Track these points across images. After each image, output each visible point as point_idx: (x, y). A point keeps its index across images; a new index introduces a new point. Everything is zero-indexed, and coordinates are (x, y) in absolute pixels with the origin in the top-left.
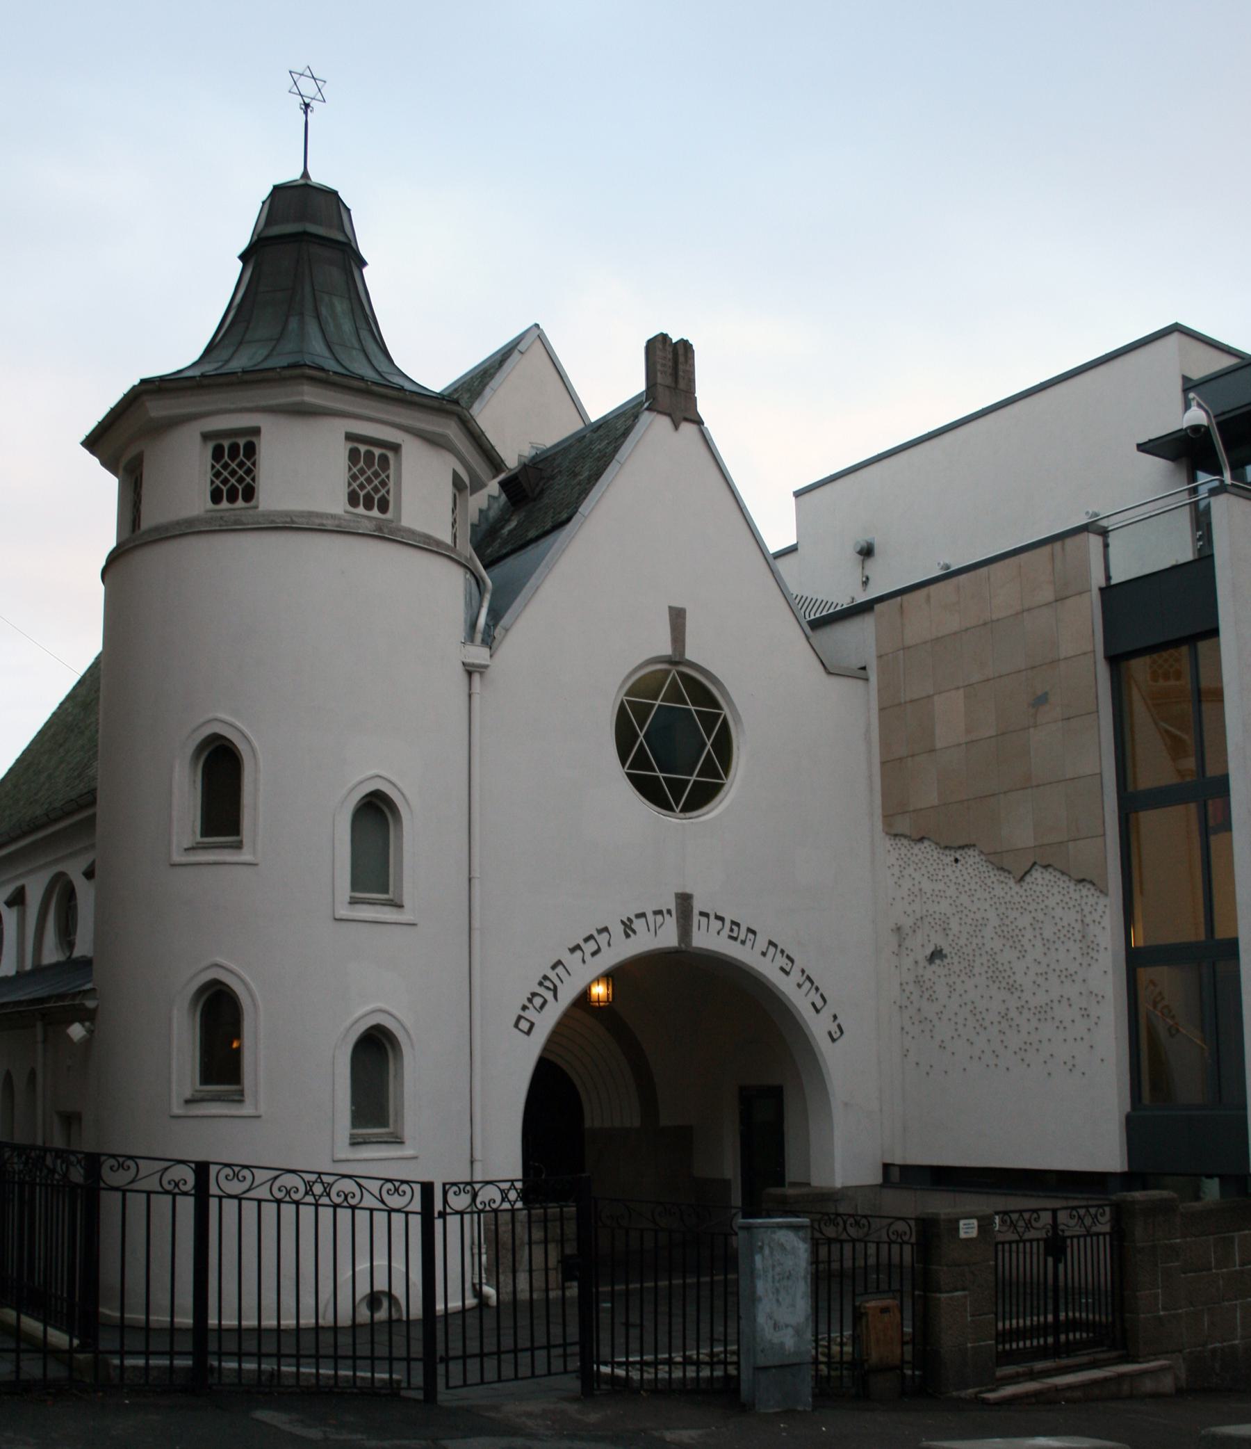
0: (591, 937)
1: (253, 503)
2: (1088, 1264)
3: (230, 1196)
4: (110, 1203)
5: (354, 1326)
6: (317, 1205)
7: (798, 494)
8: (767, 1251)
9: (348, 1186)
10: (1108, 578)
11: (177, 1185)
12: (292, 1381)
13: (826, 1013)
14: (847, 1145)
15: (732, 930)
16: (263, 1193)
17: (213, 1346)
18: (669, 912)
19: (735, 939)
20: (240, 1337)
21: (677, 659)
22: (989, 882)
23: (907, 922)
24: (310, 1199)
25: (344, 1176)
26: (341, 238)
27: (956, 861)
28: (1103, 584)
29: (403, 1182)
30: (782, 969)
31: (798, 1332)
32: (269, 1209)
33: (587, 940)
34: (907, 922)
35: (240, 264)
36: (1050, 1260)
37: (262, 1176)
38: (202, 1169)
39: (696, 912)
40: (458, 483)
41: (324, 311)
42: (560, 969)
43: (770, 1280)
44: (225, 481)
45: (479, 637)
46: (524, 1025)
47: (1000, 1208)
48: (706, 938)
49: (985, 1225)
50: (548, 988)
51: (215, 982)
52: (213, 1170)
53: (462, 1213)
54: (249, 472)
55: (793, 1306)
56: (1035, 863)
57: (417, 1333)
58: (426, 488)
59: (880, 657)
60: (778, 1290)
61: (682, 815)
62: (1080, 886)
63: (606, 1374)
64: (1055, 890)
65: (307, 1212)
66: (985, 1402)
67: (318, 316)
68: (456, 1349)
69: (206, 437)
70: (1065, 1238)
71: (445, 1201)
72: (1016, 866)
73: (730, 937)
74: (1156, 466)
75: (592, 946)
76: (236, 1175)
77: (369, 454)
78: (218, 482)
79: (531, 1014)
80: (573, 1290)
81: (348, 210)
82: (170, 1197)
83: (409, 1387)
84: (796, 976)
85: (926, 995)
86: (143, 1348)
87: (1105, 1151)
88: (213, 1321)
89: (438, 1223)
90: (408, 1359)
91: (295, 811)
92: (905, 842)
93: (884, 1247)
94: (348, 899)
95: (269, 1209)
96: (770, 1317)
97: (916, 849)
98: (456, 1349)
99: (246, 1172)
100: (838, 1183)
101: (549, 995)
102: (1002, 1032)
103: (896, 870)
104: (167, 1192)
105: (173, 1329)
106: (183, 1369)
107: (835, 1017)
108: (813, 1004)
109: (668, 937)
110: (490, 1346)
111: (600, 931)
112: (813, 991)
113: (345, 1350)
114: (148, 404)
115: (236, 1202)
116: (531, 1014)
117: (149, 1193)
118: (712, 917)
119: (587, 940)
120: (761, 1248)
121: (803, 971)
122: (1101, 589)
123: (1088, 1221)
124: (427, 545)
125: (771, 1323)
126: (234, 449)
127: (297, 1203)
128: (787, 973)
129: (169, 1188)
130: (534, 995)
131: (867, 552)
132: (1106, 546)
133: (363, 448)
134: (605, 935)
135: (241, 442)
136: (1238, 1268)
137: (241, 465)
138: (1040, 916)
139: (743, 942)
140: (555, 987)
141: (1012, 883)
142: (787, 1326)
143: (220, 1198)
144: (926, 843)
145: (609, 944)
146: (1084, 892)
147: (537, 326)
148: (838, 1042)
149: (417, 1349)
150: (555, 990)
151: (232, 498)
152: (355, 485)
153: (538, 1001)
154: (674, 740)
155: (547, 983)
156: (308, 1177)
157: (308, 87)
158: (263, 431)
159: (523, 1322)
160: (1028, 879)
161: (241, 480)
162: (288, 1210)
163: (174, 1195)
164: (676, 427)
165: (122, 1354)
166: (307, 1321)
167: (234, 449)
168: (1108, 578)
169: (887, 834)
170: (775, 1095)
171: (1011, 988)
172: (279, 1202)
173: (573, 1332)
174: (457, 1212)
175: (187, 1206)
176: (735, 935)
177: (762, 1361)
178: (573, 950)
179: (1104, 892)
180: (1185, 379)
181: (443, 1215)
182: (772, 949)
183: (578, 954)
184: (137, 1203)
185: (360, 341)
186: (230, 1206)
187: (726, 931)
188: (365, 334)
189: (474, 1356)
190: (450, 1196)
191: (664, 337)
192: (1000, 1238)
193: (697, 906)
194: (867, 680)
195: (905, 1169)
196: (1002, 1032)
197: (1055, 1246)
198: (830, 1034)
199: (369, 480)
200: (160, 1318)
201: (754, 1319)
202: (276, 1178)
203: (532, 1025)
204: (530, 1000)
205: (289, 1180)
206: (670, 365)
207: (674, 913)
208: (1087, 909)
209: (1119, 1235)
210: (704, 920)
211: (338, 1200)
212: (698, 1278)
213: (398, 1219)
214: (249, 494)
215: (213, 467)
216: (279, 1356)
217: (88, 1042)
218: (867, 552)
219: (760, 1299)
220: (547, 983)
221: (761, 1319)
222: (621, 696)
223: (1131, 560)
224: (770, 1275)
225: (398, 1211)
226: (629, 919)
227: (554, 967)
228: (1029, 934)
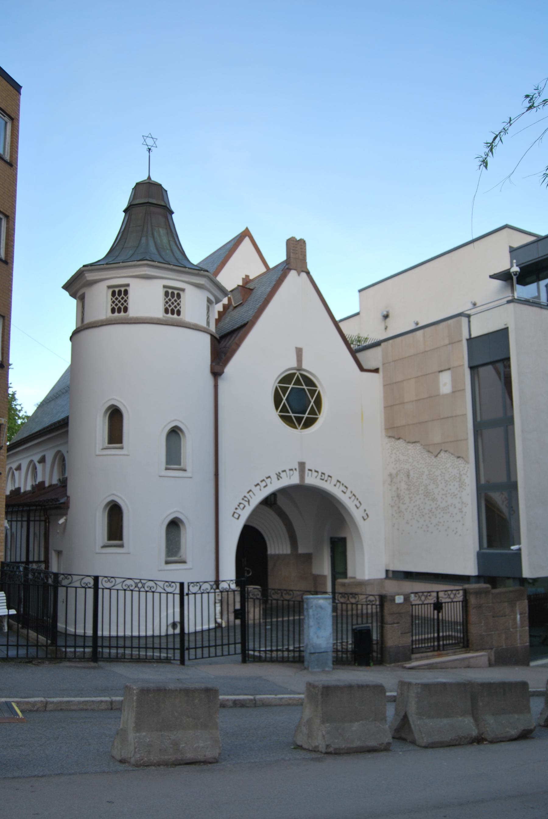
0: (264, 480)
1: (127, 314)
2: (453, 612)
3: (107, 588)
4: (61, 591)
5: (167, 635)
6: (139, 591)
7: (360, 291)
9: (151, 584)
10: (470, 335)
11: (87, 584)
13: (362, 509)
14: (369, 563)
16: (119, 587)
17: (99, 643)
18: (296, 469)
19: (323, 480)
20: (84, 640)
21: (299, 368)
22: (424, 456)
23: (394, 472)
24: (137, 589)
26: (163, 204)
28: (468, 337)
29: (172, 582)
30: (343, 491)
32: (121, 593)
33: (262, 481)
34: (394, 472)
35: (124, 214)
36: (436, 612)
37: (118, 580)
38: (96, 579)
40: (209, 301)
41: (156, 234)
42: (251, 493)
44: (116, 305)
46: (236, 516)
47: (416, 590)
48: (311, 480)
49: (407, 598)
50: (246, 501)
51: (113, 501)
52: (100, 579)
53: (195, 594)
54: (125, 301)
56: (441, 450)
57: (178, 640)
58: (195, 305)
59: (383, 364)
62: (459, 459)
63: (251, 655)
65: (136, 594)
66: (405, 668)
67: (153, 234)
68: (192, 645)
69: (109, 287)
70: (442, 603)
71: (189, 589)
72: (434, 450)
73: (321, 479)
74: (497, 283)
75: (264, 484)
76: (109, 581)
77: (173, 293)
78: (114, 305)
79: (239, 511)
80: (238, 622)
81: (166, 191)
82: (84, 589)
83: (174, 660)
84: (348, 494)
85: (401, 502)
86: (64, 645)
87: (470, 568)
88: (100, 633)
89: (186, 598)
90: (174, 649)
91: (144, 435)
92: (393, 439)
93: (364, 607)
94: (164, 468)
95: (121, 593)
97: (398, 442)
98: (192, 645)
99: (112, 579)
100: (367, 577)
101: (246, 504)
102: (430, 518)
104: (83, 587)
105: (84, 637)
106: (89, 652)
107: (365, 510)
109: (295, 480)
110: (219, 642)
111: (267, 478)
112: (356, 500)
113: (157, 646)
114: (86, 275)
115: (108, 590)
116: (239, 511)
117: (76, 588)
119: (262, 481)
121: (351, 492)
122: (467, 340)
123: (423, 598)
126: (120, 292)
127: (132, 591)
128: (345, 493)
129: (83, 585)
130: (240, 503)
131: (386, 317)
132: (469, 322)
133: (170, 291)
134: (269, 479)
135: (123, 289)
137: (122, 298)
138: (443, 471)
139: (326, 481)
141: (433, 457)
143: (103, 589)
144: (401, 440)
145: (271, 483)
146: (460, 462)
148: (366, 521)
149: (178, 646)
150: (249, 502)
151: (119, 312)
153: (242, 506)
154: (298, 400)
157: (150, 142)
158: (131, 285)
159: (232, 634)
160: (439, 456)
161: (122, 304)
162: (128, 593)
164: (299, 275)
165: (66, 647)
166: (150, 633)
167: (120, 292)
168: (470, 335)
169: (387, 436)
170: (343, 540)
171: (434, 500)
172: (125, 590)
173: (239, 640)
174: (193, 593)
175: (90, 593)
176: (323, 478)
178: (256, 486)
179: (467, 462)
180: (510, 247)
181: (188, 594)
182: (338, 484)
183: (258, 487)
184: (71, 591)
185: (170, 246)
186: (107, 592)
187: (319, 477)
188: (172, 243)
189: (206, 647)
190: (191, 588)
192: (414, 603)
193: (307, 467)
195: (394, 572)
196: (430, 518)
197: (438, 606)
198: (363, 517)
199: (173, 303)
200: (80, 631)
202: (124, 581)
203: (239, 515)
204: (239, 506)
205: (129, 582)
206: (296, 250)
208: (461, 469)
209: (465, 602)
210: (310, 472)
211: (147, 589)
213: (171, 596)
214: (126, 310)
215: (112, 299)
216: (125, 647)
218: (386, 317)
220: (246, 499)
222: (277, 384)
223: (481, 327)
225: (171, 593)
226: (279, 473)
227: (248, 492)
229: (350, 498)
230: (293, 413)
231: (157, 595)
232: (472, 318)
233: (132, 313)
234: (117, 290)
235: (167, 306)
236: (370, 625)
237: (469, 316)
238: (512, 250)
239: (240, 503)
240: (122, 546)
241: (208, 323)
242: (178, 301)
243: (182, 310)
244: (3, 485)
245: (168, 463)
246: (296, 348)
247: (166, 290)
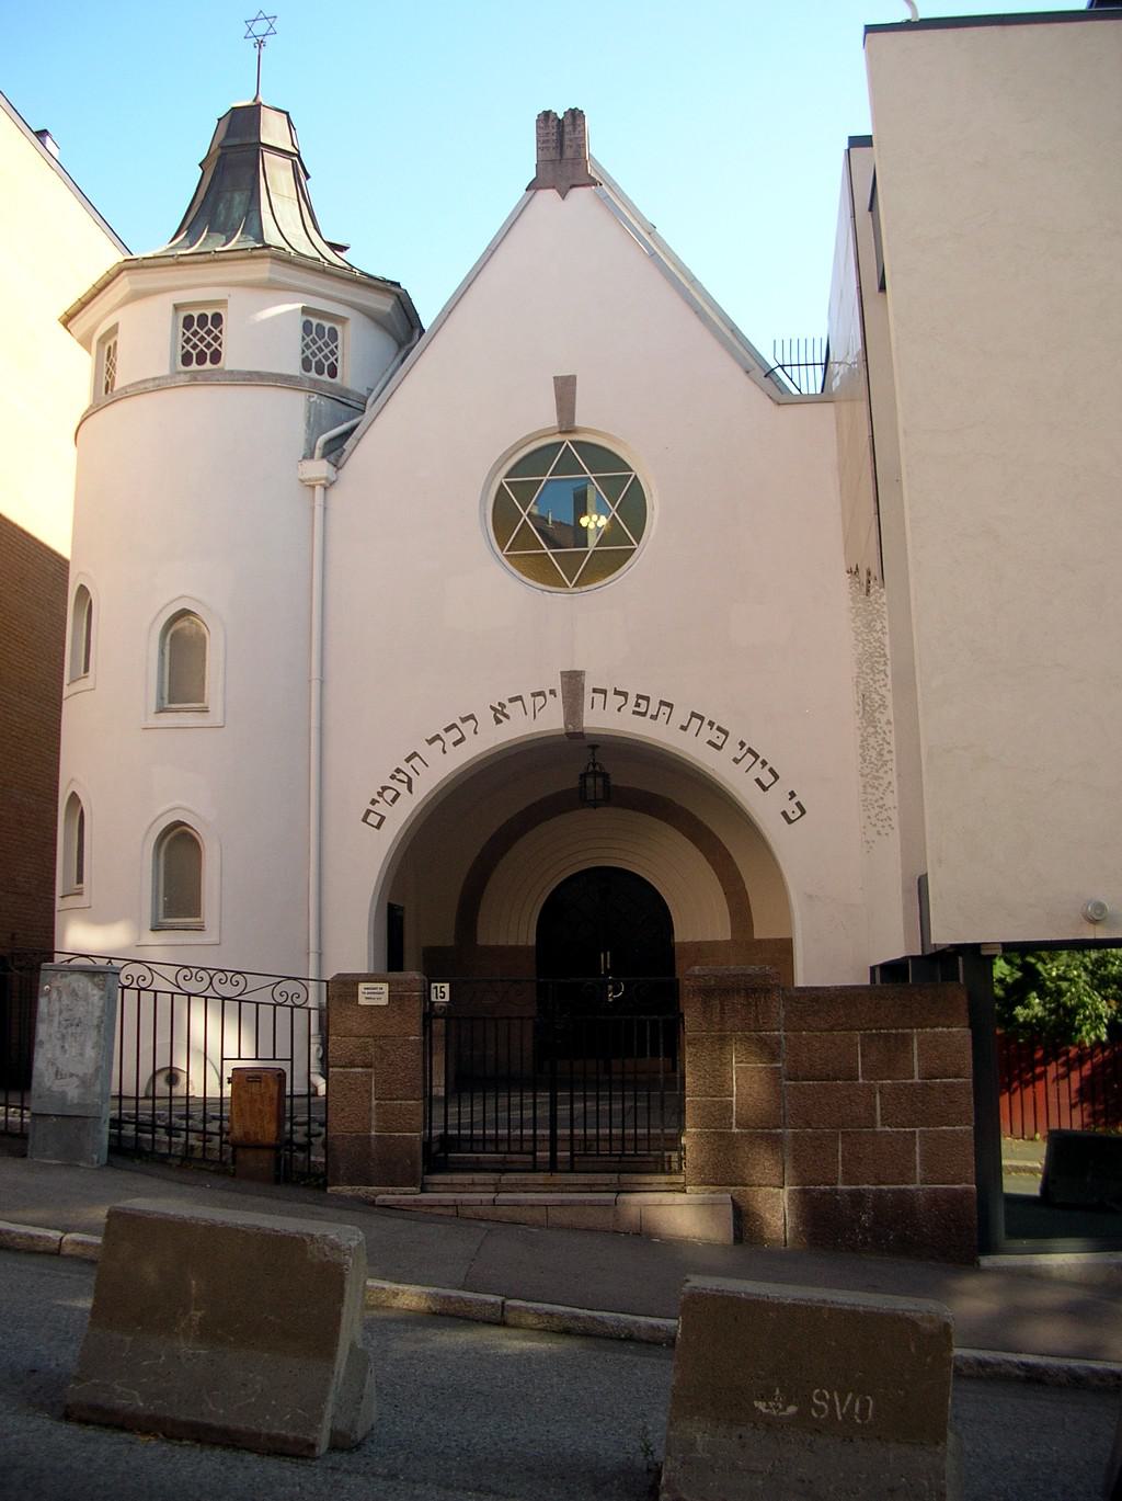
0: (454, 726)
8: (54, 995)
15: (638, 705)
19: (644, 714)
25: (289, 978)
33: (447, 730)
43: (56, 1024)
44: (195, 347)
45: (318, 453)
48: (600, 719)
60: (63, 1037)
61: (576, 589)
75: (455, 735)
79: (381, 808)
84: (732, 749)
101: (402, 788)
108: (758, 781)
109: (552, 720)
111: (464, 720)
116: (381, 808)
119: (447, 730)
125: (52, 1071)
130: (384, 788)
133: (315, 321)
135: (209, 313)
136: (917, 1080)
140: (410, 779)
142: (72, 1075)
152: (308, 353)
153: (389, 795)
163: (275, 1006)
178: (430, 742)
183: (439, 742)
193: (589, 683)
207: (559, 693)
210: (599, 697)
212: (572, 1092)
219: (42, 1043)
224: (56, 1020)
227: (408, 760)
229: (736, 761)
230: (548, 481)
234: (196, 314)
236: (286, 1066)
242: (333, 346)
243: (339, 366)
246: (563, 198)
247: (305, 318)
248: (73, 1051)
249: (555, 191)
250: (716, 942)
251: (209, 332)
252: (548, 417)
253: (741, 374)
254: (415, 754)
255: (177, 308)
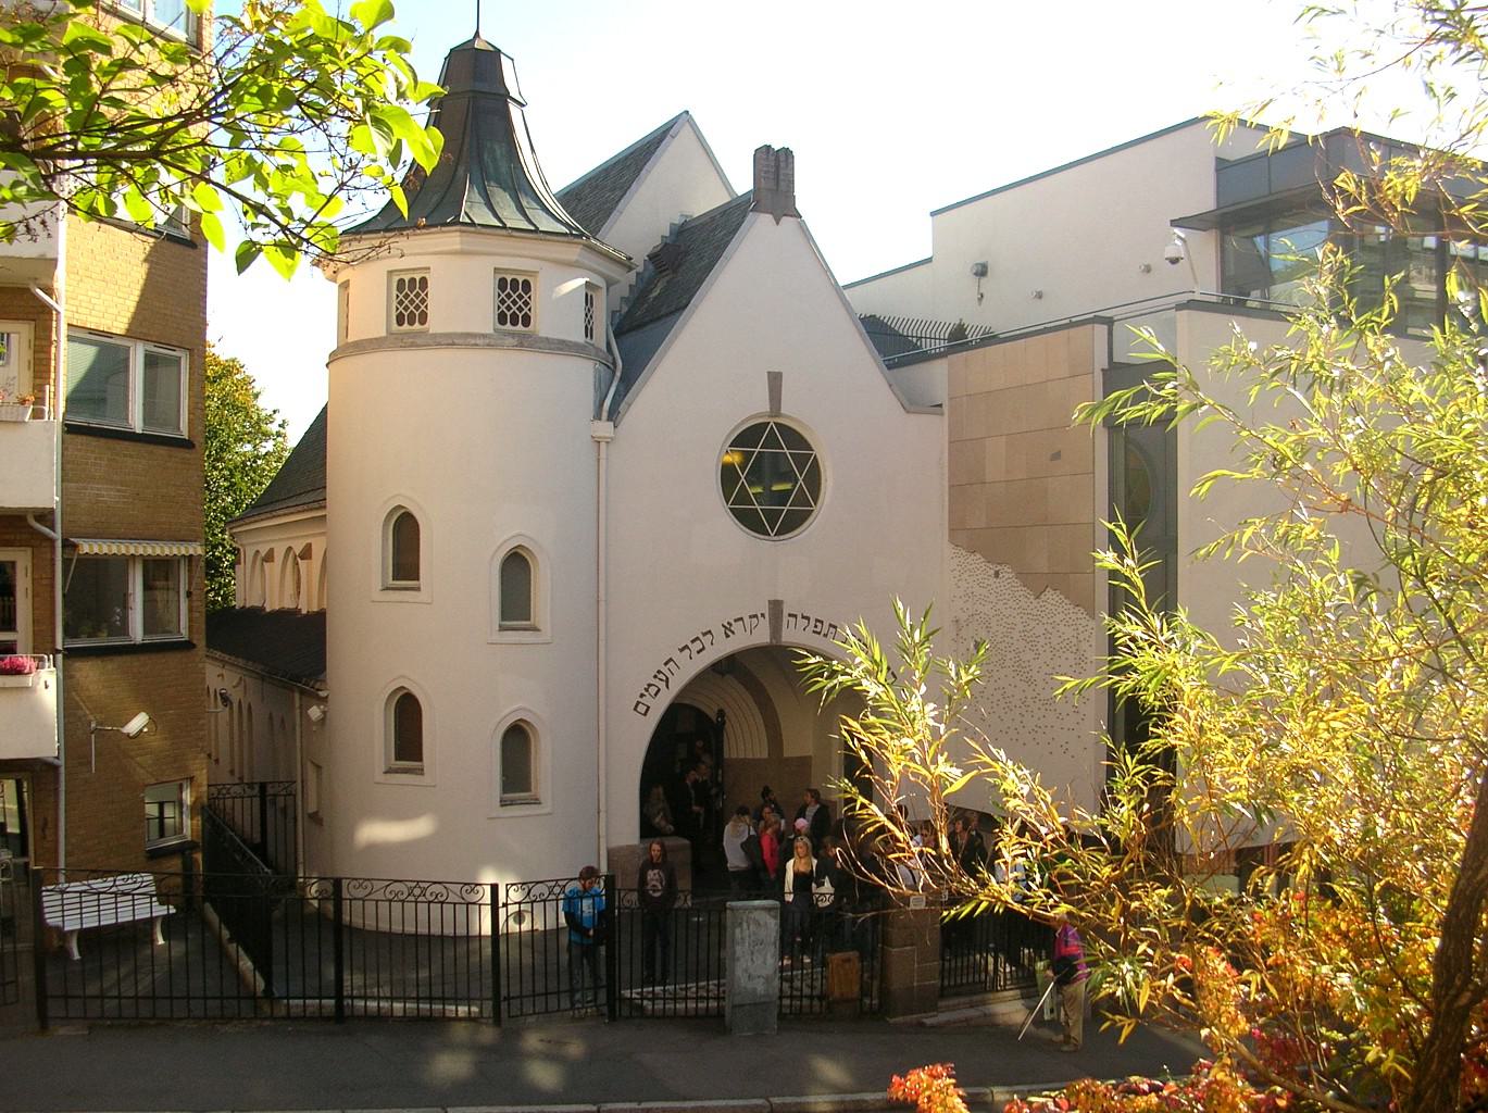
6: (416, 902)
7: (933, 214)
8: (745, 925)
9: (437, 888)
12: (401, 1014)
18: (763, 615)
23: (963, 617)
24: (412, 898)
27: (997, 574)
31: (768, 980)
34: (963, 617)
39: (785, 614)
45: (605, 415)
46: (642, 709)
48: (791, 635)
55: (765, 963)
58: (563, 292)
64: (1060, 610)
75: (698, 645)
79: (647, 700)
91: (459, 565)
96: (746, 970)
101: (662, 685)
103: (956, 573)
109: (761, 636)
111: (704, 634)
116: (647, 700)
118: (799, 617)
119: (693, 641)
120: (741, 924)
124: (562, 347)
130: (650, 685)
137: (406, 308)
139: (825, 635)
147: (687, 112)
153: (653, 690)
154: (770, 477)
155: (661, 676)
156: (409, 884)
161: (520, 309)
162: (397, 906)
171: (1029, 681)
177: (737, 1000)
178: (682, 650)
183: (687, 651)
191: (768, 147)
194: (942, 414)
201: (733, 972)
205: (396, 887)
206: (775, 167)
207: (767, 616)
210: (792, 619)
214: (423, 319)
217: (323, 721)
218: (982, 271)
219: (738, 959)
220: (661, 676)
221: (739, 972)
227: (666, 664)
228: (1042, 640)
231: (448, 909)
232: (1116, 326)
233: (435, 324)
235: (503, 308)
237: (1110, 322)
238: (1222, 166)
239: (650, 685)
240: (421, 771)
241: (589, 332)
243: (532, 314)
244: (200, 665)
245: (504, 616)
248: (759, 962)
249: (771, 216)
250: (759, 760)
251: (520, 297)
252: (765, 407)
253: (887, 386)
254: (671, 660)
255: (496, 270)
